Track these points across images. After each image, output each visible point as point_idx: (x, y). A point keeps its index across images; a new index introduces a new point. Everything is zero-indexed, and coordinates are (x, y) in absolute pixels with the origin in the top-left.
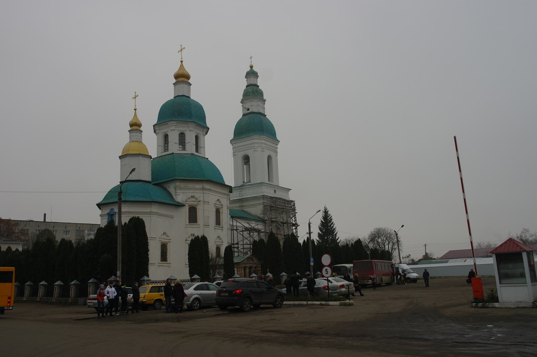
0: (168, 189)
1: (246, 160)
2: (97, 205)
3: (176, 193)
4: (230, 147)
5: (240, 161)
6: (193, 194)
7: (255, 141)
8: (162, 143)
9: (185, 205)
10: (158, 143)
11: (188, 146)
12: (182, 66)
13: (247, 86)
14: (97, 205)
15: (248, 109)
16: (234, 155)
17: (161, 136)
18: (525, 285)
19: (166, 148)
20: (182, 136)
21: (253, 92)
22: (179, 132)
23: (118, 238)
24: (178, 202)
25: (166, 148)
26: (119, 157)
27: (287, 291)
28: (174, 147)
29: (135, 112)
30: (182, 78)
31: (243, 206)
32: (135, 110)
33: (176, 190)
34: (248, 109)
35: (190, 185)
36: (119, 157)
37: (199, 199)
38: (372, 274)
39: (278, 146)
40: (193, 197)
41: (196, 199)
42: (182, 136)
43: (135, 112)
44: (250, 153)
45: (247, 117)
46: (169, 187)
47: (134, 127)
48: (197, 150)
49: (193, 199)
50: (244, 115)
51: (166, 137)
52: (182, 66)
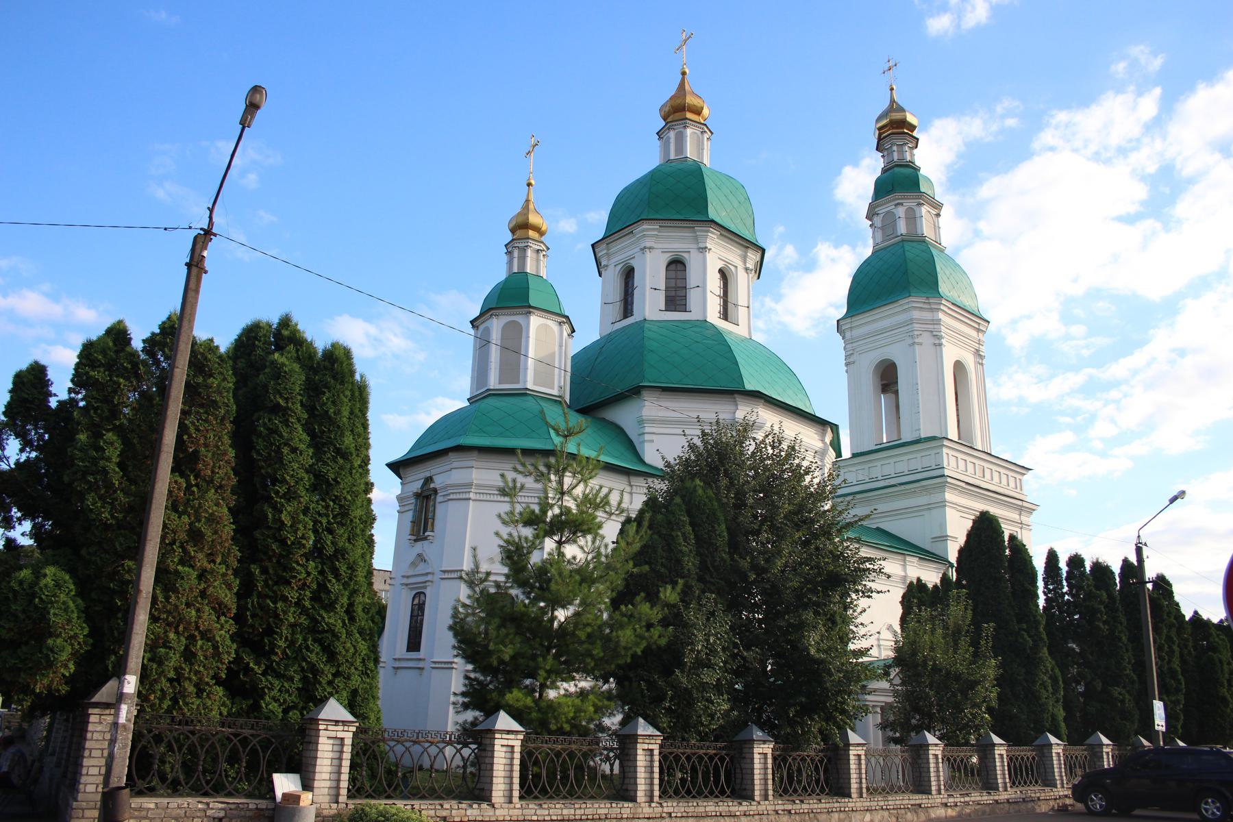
1: (887, 378)
2: (388, 465)
4: (839, 341)
5: (869, 381)
7: (916, 314)
8: (616, 295)
10: (604, 294)
11: (693, 297)
14: (388, 465)
16: (847, 365)
17: (614, 274)
18: (397, 664)
19: (627, 310)
20: (677, 265)
22: (664, 260)
26: (472, 322)
27: (980, 759)
29: (683, 79)
30: (678, 112)
36: (472, 322)
42: (677, 265)
43: (683, 79)
44: (895, 353)
47: (519, 233)
48: (725, 315)
51: (628, 274)
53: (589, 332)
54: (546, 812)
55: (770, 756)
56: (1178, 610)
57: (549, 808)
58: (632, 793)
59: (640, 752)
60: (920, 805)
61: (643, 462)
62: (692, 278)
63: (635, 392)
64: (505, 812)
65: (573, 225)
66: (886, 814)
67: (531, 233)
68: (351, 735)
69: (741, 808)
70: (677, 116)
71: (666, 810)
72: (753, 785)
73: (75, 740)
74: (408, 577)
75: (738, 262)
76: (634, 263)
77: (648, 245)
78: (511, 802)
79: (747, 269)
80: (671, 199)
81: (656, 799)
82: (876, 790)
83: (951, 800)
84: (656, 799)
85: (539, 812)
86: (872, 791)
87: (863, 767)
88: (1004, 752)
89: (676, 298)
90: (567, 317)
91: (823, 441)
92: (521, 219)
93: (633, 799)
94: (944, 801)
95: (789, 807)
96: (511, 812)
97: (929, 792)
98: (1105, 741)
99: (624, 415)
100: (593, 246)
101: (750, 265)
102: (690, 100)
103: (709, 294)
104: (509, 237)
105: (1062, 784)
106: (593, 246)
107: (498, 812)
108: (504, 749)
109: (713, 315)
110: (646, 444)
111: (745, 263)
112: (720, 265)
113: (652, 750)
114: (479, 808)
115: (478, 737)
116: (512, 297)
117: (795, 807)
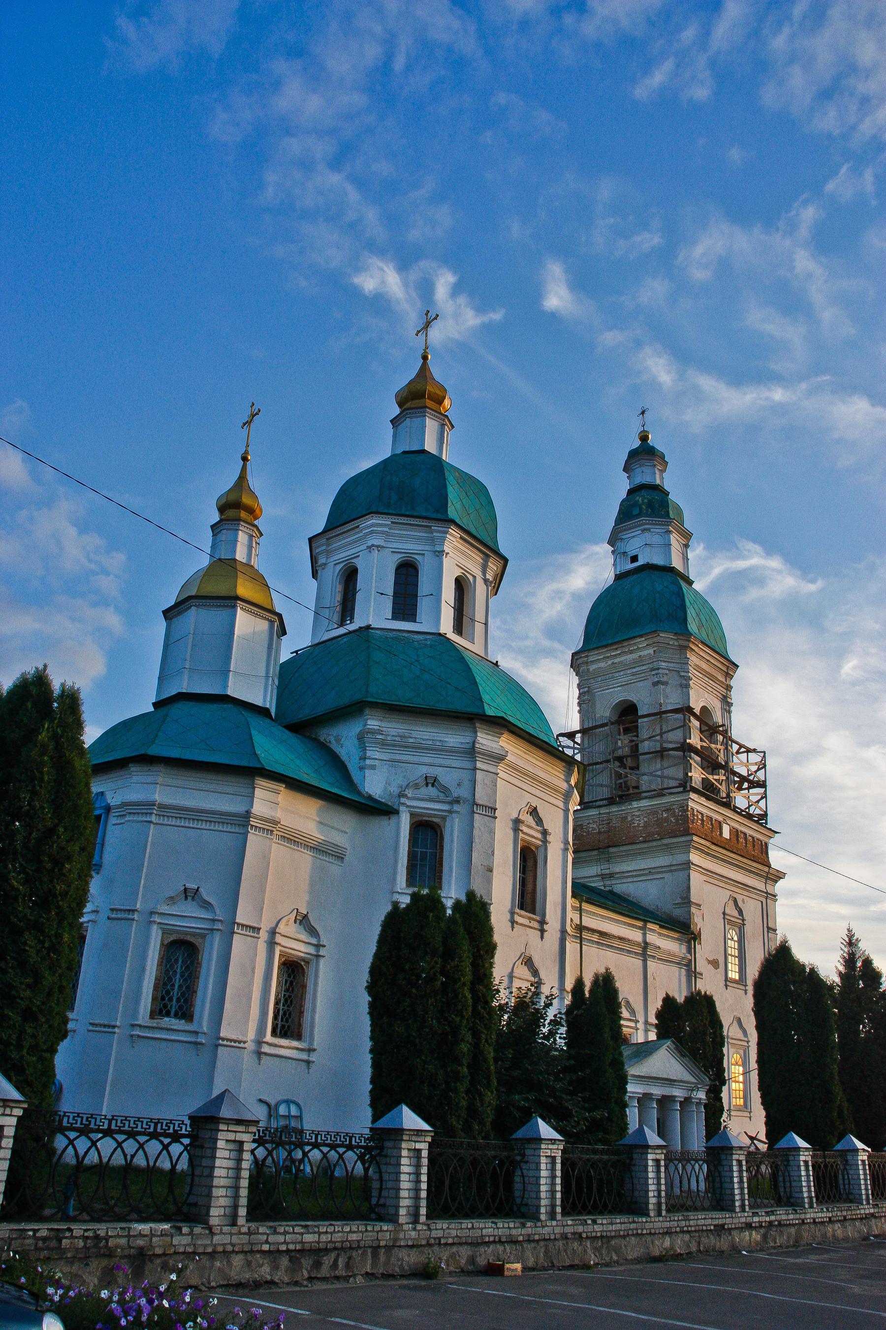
0: (334, 746)
3: (364, 758)
6: (432, 771)
9: (397, 812)
11: (424, 606)
12: (424, 370)
13: (631, 492)
15: (634, 559)
17: (332, 574)
20: (407, 572)
21: (650, 505)
23: (150, 952)
24: (370, 798)
25: (347, 608)
28: (375, 611)
31: (611, 876)
32: (245, 459)
33: (364, 749)
34: (634, 559)
35: (424, 732)
37: (456, 792)
38: (137, 1020)
39: (732, 683)
40: (431, 781)
41: (445, 790)
42: (407, 572)
45: (627, 582)
46: (338, 739)
47: (231, 513)
48: (459, 628)
49: (432, 791)
50: (619, 577)
51: (350, 576)
52: (424, 370)
53: (299, 638)
54: (281, 1239)
55: (559, 1160)
56: (756, 1004)
57: (285, 1233)
58: (392, 1211)
59: (221, 1144)
60: (723, 1225)
61: (359, 793)
62: (424, 586)
63: (353, 710)
64: (226, 1239)
65: (294, 510)
66: (687, 1237)
67: (243, 514)
68: (13, 1121)
69: (524, 1231)
70: (416, 403)
71: (434, 1234)
72: (539, 1198)
73: (693, 1229)
74: (117, 910)
75: (478, 573)
76: (358, 563)
77: (376, 542)
78: (234, 1224)
79: (486, 581)
80: (410, 490)
81: (423, 1219)
82: (673, 1206)
83: (756, 1219)
84: (423, 1219)
85: (272, 1239)
86: (672, 1209)
87: (663, 1175)
88: (809, 1158)
89: (405, 601)
90: (280, 616)
91: (568, 781)
92: (233, 497)
93: (393, 1219)
94: (749, 1220)
95: (580, 1229)
96: (235, 1239)
97: (731, 1209)
98: (802, 1143)
99: (344, 738)
100: (311, 540)
101: (490, 577)
102: (246, 500)
103: (443, 604)
104: (216, 517)
105: (868, 1199)
106: (311, 540)
107: (216, 1239)
108: (231, 1146)
109: (446, 626)
110: (368, 772)
111: (484, 573)
112: (458, 572)
113: (419, 1151)
114: (191, 1233)
115: (383, 1143)
116: (214, 593)
117: (586, 1229)
